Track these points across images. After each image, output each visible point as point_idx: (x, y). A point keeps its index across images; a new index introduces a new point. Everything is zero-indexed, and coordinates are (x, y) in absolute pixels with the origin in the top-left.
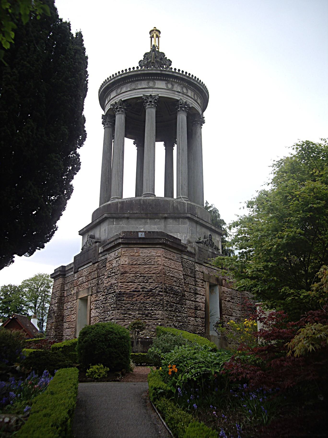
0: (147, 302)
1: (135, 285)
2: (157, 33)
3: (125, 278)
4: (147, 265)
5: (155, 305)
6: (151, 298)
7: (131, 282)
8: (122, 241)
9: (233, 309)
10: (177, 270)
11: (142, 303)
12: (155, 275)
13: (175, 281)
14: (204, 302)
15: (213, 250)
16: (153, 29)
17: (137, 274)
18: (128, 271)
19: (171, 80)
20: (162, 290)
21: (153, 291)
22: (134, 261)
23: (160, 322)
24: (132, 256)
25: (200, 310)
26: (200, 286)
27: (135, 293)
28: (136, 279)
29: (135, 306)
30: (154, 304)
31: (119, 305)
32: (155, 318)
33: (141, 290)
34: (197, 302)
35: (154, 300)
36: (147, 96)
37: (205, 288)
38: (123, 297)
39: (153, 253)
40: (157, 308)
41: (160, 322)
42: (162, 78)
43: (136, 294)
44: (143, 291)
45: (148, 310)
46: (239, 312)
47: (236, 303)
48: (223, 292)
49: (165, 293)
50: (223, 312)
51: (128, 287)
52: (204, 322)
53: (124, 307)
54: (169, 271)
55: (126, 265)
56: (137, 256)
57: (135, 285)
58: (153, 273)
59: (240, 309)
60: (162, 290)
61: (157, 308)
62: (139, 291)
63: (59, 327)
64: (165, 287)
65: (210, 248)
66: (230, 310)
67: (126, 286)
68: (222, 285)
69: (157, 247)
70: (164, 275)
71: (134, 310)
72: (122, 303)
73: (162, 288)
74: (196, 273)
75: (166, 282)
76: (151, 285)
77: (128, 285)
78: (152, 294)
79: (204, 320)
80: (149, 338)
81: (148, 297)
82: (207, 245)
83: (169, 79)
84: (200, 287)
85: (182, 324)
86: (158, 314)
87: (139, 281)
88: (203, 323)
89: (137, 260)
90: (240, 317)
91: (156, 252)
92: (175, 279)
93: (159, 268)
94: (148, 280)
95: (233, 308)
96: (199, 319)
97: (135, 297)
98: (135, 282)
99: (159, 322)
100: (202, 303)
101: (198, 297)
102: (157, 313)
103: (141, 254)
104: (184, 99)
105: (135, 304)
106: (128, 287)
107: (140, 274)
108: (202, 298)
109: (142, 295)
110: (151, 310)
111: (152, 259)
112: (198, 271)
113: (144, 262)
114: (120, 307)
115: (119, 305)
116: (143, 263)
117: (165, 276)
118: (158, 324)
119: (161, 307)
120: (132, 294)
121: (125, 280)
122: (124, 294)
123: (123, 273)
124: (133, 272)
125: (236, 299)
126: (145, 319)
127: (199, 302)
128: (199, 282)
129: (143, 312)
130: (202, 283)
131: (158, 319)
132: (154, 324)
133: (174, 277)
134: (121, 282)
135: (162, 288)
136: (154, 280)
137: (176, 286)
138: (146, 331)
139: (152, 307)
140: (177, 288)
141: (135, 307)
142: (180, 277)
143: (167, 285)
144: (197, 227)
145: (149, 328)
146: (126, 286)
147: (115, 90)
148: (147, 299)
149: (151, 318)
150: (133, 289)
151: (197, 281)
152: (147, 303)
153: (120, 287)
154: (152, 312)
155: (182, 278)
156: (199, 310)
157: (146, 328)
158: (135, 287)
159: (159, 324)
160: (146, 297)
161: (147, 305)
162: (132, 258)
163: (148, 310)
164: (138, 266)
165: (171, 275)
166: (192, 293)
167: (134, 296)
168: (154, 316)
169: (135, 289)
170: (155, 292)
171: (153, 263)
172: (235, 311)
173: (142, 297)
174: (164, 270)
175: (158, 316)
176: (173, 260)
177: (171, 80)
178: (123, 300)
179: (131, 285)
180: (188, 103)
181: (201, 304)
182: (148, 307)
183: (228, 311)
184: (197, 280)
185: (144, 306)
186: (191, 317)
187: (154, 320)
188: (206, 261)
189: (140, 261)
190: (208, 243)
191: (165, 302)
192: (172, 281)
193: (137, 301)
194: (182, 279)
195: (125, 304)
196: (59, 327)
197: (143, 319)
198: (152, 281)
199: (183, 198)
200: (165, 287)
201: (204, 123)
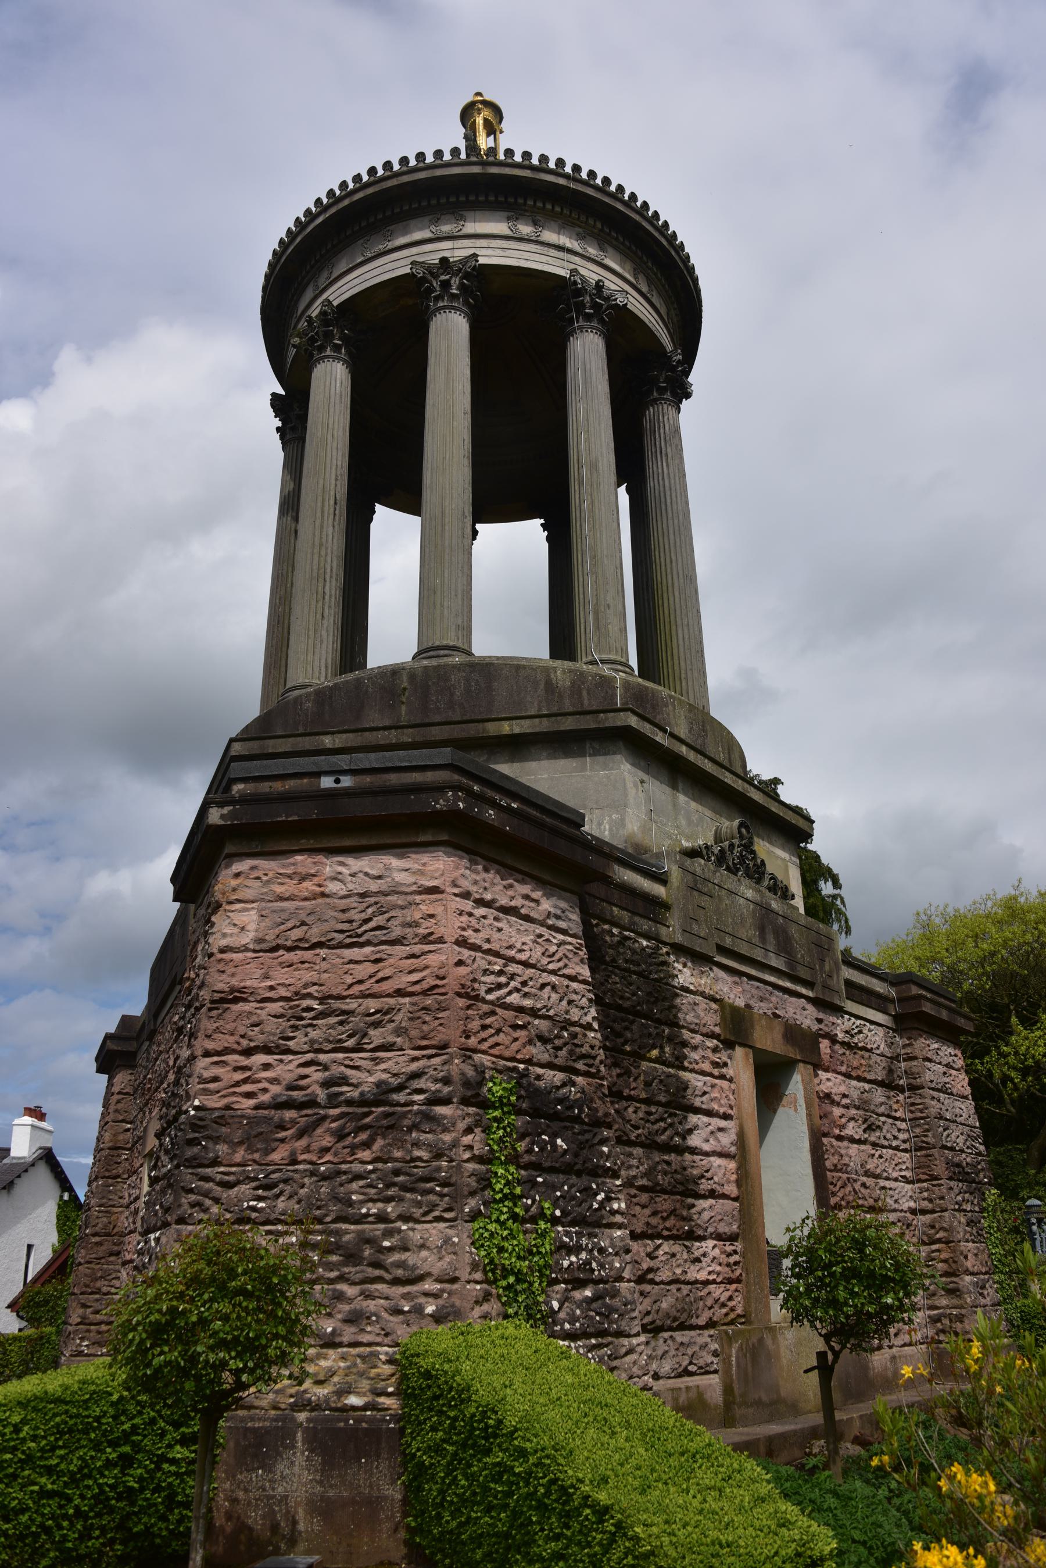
0: (357, 1167)
1: (287, 1069)
2: (486, 113)
3: (230, 1026)
4: (362, 945)
5: (405, 1188)
6: (379, 1143)
7: (267, 1050)
8: (222, 817)
9: (877, 1177)
10: (553, 972)
11: (324, 1178)
12: (407, 1000)
13: (543, 1039)
14: (733, 1149)
15: (762, 895)
16: (470, 98)
17: (305, 1003)
18: (255, 983)
19: (530, 202)
20: (446, 1090)
21: (395, 1097)
22: (289, 925)
23: (436, 1296)
24: (281, 899)
25: (712, 1194)
26: (706, 1066)
27: (289, 1114)
28: (295, 1028)
29: (281, 1193)
30: (401, 1178)
31: (191, 1191)
32: (400, 1272)
33: (321, 1095)
34: (693, 1151)
35: (398, 1154)
36: (429, 268)
37: (731, 1080)
38: (217, 1140)
39: (401, 877)
40: (419, 1205)
41: (436, 1296)
42: (492, 198)
43: (294, 1122)
44: (333, 1100)
45: (361, 1219)
46: (909, 1187)
47: (890, 1147)
48: (828, 1096)
49: (472, 1110)
50: (834, 1194)
51: (245, 1081)
52: (736, 1258)
53: (217, 1200)
54: (503, 979)
55: (245, 949)
56: (306, 899)
57: (287, 1069)
58: (400, 993)
59: (908, 1174)
60: (446, 1090)
61: (419, 1205)
62: (312, 1103)
63: (98, 1284)
64: (470, 1073)
65: (746, 881)
66: (864, 1179)
67: (239, 1076)
68: (817, 1065)
69: (422, 839)
70: (462, 1002)
71: (280, 1221)
72: (207, 1179)
73: (446, 1081)
74: (678, 1001)
75: (473, 1041)
76: (382, 1060)
77: (249, 1069)
78: (387, 1115)
79: (738, 1246)
80: (364, 1408)
81: (363, 1136)
82: (728, 869)
83: (521, 201)
84: (703, 1073)
85: (596, 1298)
86: (423, 1246)
87: (312, 1042)
88: (728, 1265)
89: (308, 920)
90: (913, 1212)
91: (416, 866)
92: (542, 1025)
93: (430, 956)
94: (365, 1035)
95: (878, 1171)
96: (710, 1243)
97: (282, 1140)
98: (288, 1051)
99: (426, 1294)
100: (721, 1155)
101: (696, 1127)
102: (416, 1237)
103: (333, 887)
104: (591, 274)
105: (285, 1181)
106: (245, 1081)
107: (322, 1000)
108: (721, 1130)
109: (326, 1125)
110: (382, 1218)
111: (395, 907)
112: (687, 990)
113: (345, 926)
114: (193, 1205)
115: (191, 1191)
116: (341, 937)
117: (469, 1007)
118: (418, 1310)
119: (442, 1195)
120: (267, 1119)
121: (229, 1041)
122: (220, 1121)
123: (223, 1001)
124: (283, 992)
125: (888, 1129)
126: (342, 1278)
127: (707, 1154)
128: (695, 1048)
129: (330, 1233)
130: (715, 1050)
131: (421, 1278)
132: (398, 1312)
133: (534, 1012)
134: (207, 1054)
135: (446, 1081)
136: (399, 1032)
137: (550, 1066)
138: (343, 1358)
139: (388, 1200)
140: (559, 1077)
141: (281, 1204)
142: (575, 1015)
143: (486, 1060)
144: (675, 799)
145: (365, 1338)
146: (239, 1076)
147: (312, 284)
148: (353, 1148)
149: (377, 1272)
150: (275, 1089)
151: (685, 1044)
152: (358, 1177)
153: (203, 1081)
154: (388, 1234)
155: (589, 1018)
156: (704, 1197)
157: (345, 1339)
158: (288, 1077)
159: (430, 1309)
160: (349, 1140)
161: (355, 1186)
162: (283, 910)
163: (361, 1219)
164: (308, 955)
165: (514, 999)
166: (659, 1104)
167: (282, 1134)
168: (396, 1257)
169: (291, 1088)
170: (406, 1104)
171: (397, 932)
172: (887, 1184)
173: (327, 1141)
174: (462, 970)
175: (424, 1253)
176: (527, 918)
177: (530, 202)
178: (215, 1163)
179: (267, 1066)
180: (606, 293)
181: (716, 1161)
182: (362, 1203)
183: (857, 1186)
184: (686, 1034)
185: (335, 1198)
186: (659, 1236)
187: (396, 1282)
188: (728, 942)
189: (327, 927)
190: (731, 860)
191: (471, 1166)
192: (521, 1034)
193: (294, 1162)
194: (588, 1027)
195: (228, 1185)
196: (98, 1284)
197: (331, 1281)
198: (391, 1039)
199: (603, 662)
200: (470, 1073)
201: (688, 396)
